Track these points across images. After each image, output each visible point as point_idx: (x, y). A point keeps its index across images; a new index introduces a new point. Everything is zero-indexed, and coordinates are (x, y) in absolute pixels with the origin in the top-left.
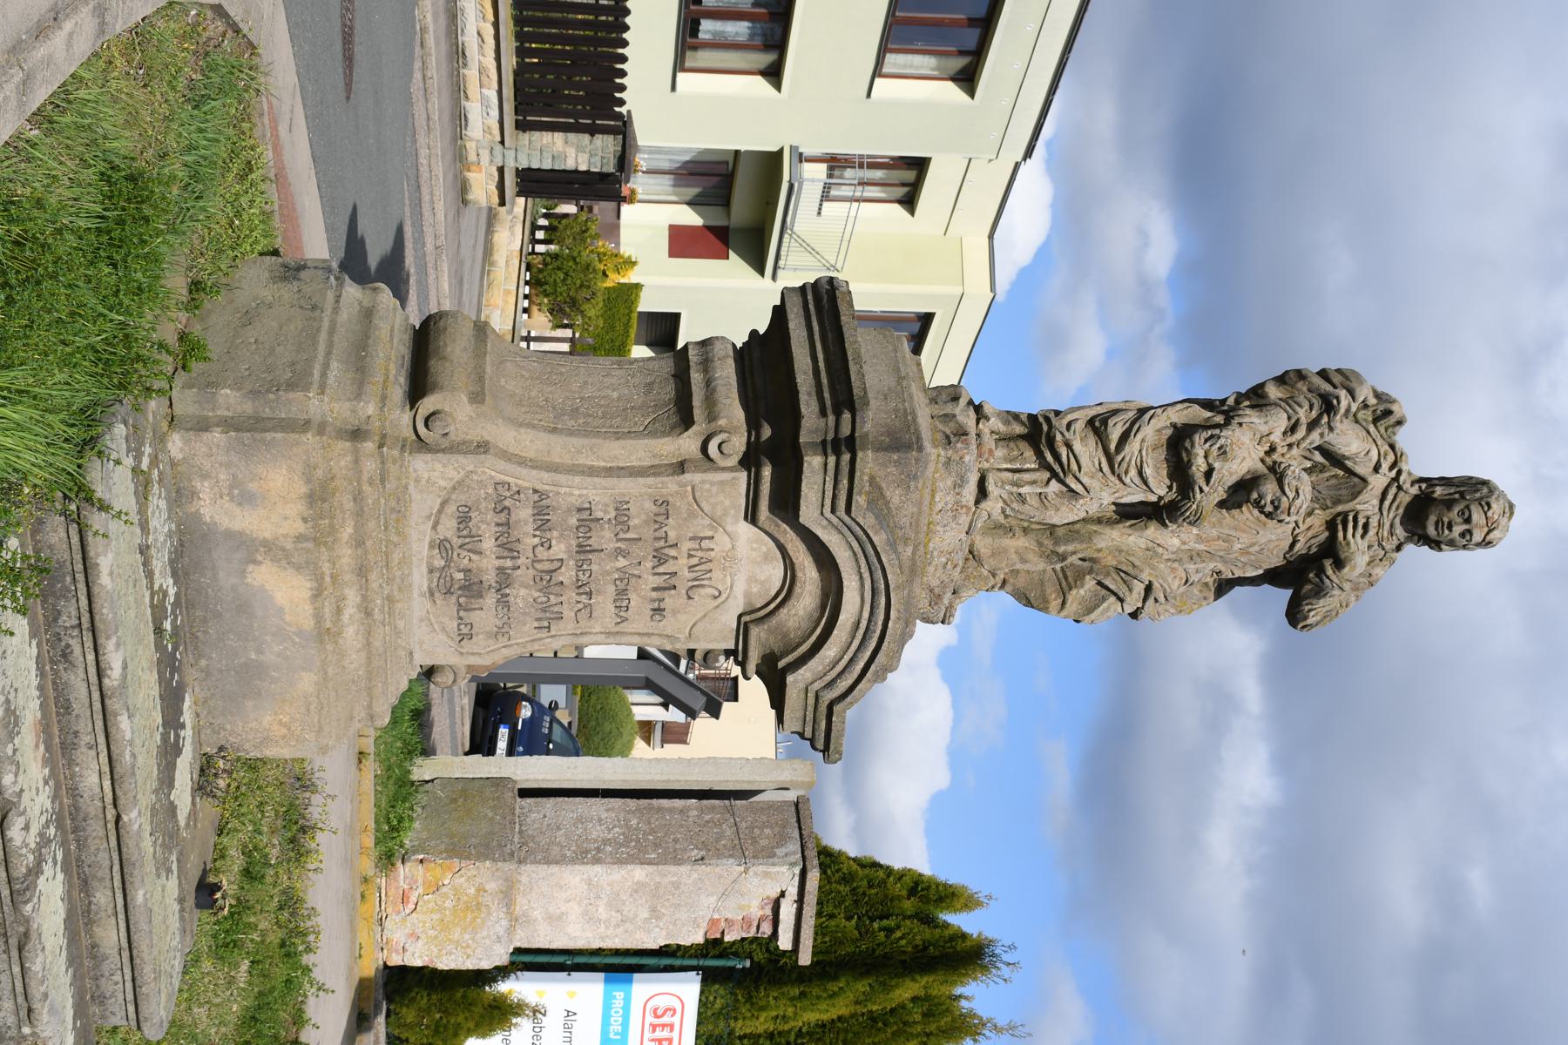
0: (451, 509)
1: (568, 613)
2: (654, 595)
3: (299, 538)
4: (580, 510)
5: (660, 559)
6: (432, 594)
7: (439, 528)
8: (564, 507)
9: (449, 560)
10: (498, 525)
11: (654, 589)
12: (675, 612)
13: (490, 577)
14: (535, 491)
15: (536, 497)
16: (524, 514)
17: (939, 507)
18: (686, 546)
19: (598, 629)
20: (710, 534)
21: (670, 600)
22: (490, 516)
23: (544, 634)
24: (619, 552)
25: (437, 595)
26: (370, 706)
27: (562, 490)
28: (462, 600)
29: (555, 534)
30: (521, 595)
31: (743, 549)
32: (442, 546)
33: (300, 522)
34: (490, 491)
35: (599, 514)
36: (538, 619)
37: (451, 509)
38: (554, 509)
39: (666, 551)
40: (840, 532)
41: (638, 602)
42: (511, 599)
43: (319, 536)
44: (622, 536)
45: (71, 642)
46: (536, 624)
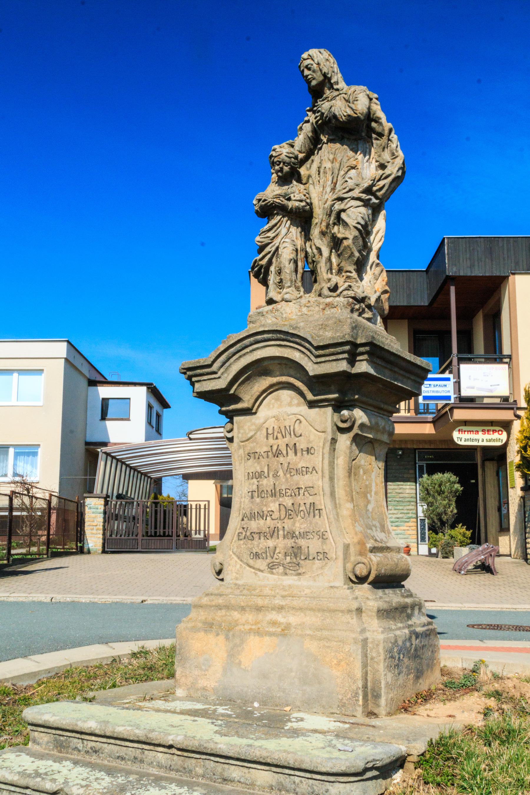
0: (251, 562)
1: (311, 499)
2: (299, 454)
3: (227, 638)
4: (252, 497)
5: (278, 454)
6: (300, 574)
7: (262, 568)
8: (251, 505)
9: (279, 564)
10: (260, 539)
11: (296, 453)
12: (309, 442)
13: (290, 542)
14: (243, 520)
15: (245, 519)
16: (254, 525)
17: (274, 319)
18: (271, 441)
19: (320, 483)
20: (265, 430)
21: (302, 445)
22: (255, 542)
23: (324, 512)
24: (276, 476)
25: (299, 571)
26: (342, 611)
27: (242, 506)
28: (303, 558)
29: (264, 509)
30: (299, 525)
31: (274, 412)
32: (271, 567)
33: (218, 637)
34: (242, 542)
35: (255, 487)
36: (314, 516)
37: (251, 562)
38: (251, 510)
39: (274, 451)
40: (230, 366)
41: (301, 462)
42: (302, 531)
43: (228, 630)
44: (266, 474)
45: (89, 746)
46: (317, 517)
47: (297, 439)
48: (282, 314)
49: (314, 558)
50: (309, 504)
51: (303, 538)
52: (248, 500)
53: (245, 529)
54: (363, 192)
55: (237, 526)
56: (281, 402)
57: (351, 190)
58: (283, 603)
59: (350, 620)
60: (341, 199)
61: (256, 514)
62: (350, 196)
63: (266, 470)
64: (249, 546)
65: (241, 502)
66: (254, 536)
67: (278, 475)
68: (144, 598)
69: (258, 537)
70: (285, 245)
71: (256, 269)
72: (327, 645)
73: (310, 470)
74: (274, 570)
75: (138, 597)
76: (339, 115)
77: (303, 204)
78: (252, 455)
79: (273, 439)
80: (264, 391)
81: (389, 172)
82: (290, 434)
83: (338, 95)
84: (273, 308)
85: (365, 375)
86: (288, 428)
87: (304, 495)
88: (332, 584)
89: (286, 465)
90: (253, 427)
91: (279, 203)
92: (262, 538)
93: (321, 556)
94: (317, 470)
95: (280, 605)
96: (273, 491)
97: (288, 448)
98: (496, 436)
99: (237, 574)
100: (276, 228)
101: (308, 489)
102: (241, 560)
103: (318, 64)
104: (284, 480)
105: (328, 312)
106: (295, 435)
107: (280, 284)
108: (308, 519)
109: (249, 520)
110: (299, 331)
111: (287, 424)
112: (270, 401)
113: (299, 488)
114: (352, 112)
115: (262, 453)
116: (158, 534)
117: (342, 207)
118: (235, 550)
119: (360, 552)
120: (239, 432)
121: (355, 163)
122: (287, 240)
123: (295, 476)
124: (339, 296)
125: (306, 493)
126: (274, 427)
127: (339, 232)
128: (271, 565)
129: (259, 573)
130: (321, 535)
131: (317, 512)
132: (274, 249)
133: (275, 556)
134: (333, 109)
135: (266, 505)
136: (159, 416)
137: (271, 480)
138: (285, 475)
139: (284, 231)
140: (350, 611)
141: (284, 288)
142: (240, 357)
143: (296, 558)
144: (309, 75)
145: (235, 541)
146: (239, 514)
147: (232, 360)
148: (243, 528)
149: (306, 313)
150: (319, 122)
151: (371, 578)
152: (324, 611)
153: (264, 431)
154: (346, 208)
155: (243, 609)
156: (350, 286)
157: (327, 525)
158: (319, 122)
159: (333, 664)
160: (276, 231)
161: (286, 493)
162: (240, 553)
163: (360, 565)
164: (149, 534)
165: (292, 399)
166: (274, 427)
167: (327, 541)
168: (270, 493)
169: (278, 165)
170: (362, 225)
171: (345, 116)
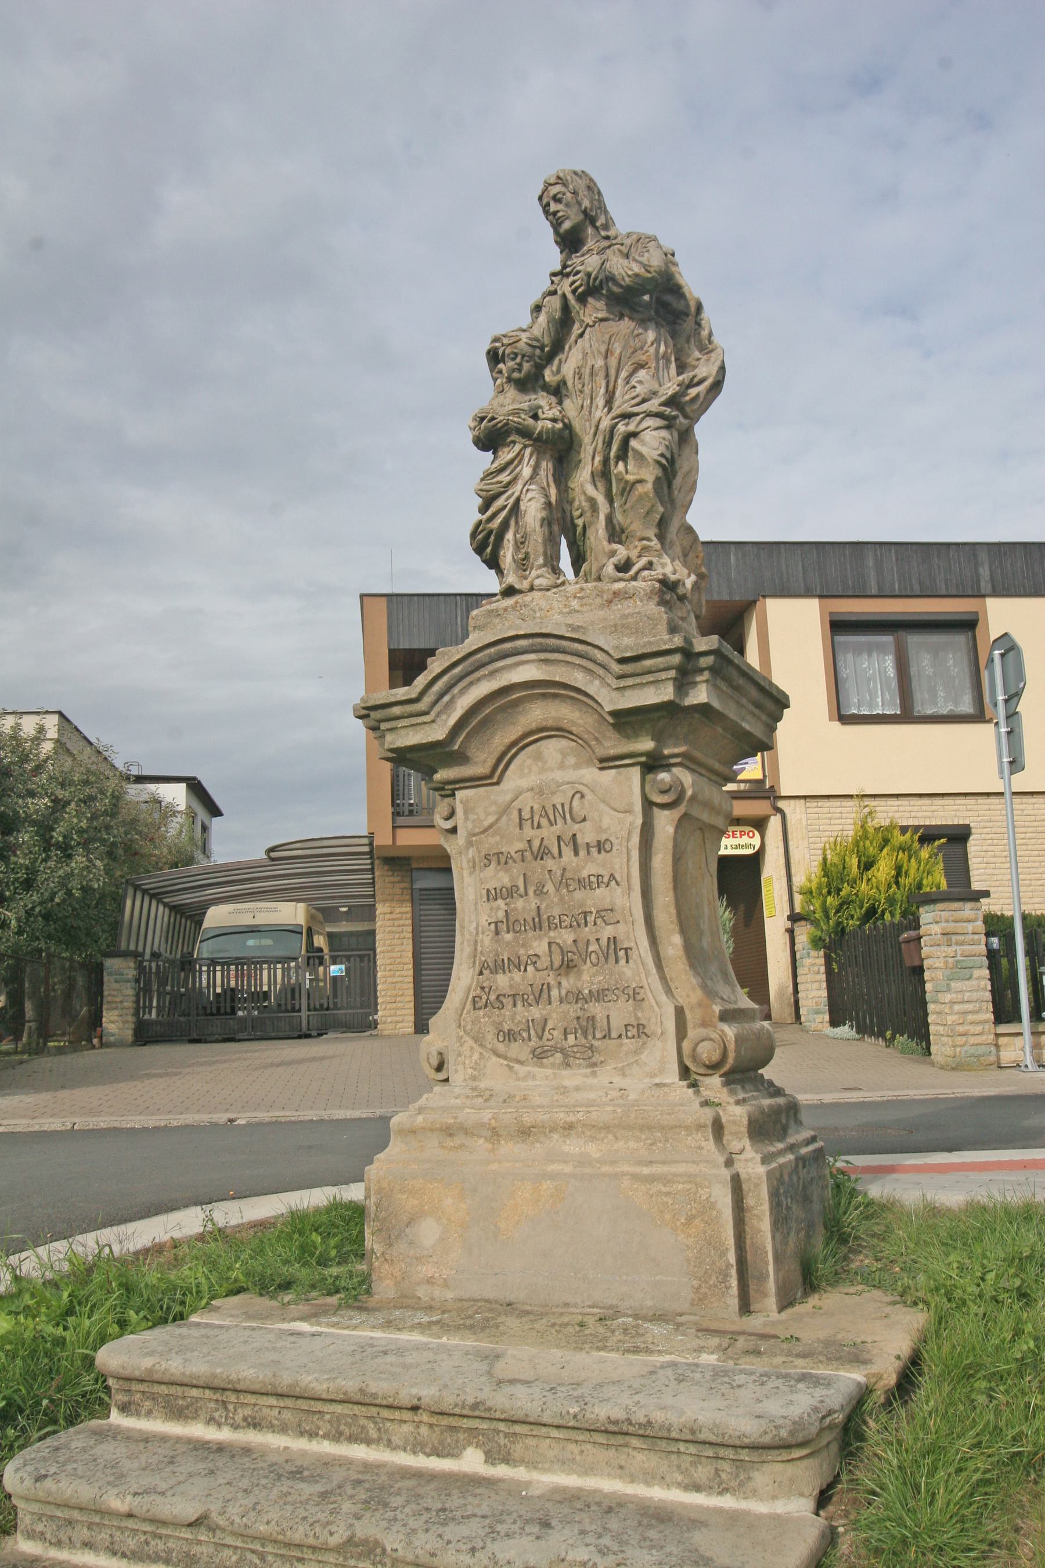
0: (501, 1047)
1: (608, 932)
2: (582, 853)
4: (497, 933)
5: (542, 853)
6: (595, 1065)
9: (555, 1049)
10: (515, 1005)
11: (576, 854)
12: (600, 830)
13: (573, 1010)
14: (481, 973)
15: (485, 972)
18: (529, 832)
21: (587, 835)
22: (507, 1012)
23: (634, 955)
24: (540, 892)
25: (594, 1060)
27: (479, 948)
29: (522, 952)
34: (481, 1013)
35: (501, 915)
36: (617, 961)
37: (501, 1047)
38: (497, 955)
47: (577, 826)
48: (534, 611)
49: (620, 1036)
50: (606, 940)
51: (598, 1000)
52: (489, 938)
53: (487, 990)
54: (662, 404)
55: (471, 985)
56: (545, 763)
57: (644, 401)
58: (571, 1118)
59: (703, 1144)
60: (626, 416)
61: (506, 962)
62: (645, 409)
63: (521, 884)
64: (496, 1018)
65: (476, 941)
66: (505, 1001)
67: (545, 890)
68: (232, 1116)
69: (512, 1003)
70: (530, 495)
71: (480, 536)
72: (664, 1189)
73: (606, 880)
74: (545, 1060)
75: (220, 1115)
76: (620, 274)
77: (559, 425)
78: (498, 858)
79: (533, 828)
80: (513, 744)
81: (704, 374)
82: (564, 818)
83: (609, 247)
84: (516, 603)
85: (704, 709)
86: (559, 807)
87: (595, 924)
88: (657, 1080)
89: (559, 873)
90: (493, 808)
91: (519, 423)
92: (519, 1004)
93: (633, 1032)
94: (618, 879)
95: (566, 1122)
96: (537, 920)
97: (562, 843)
98: (745, 840)
99: (475, 1069)
100: (512, 467)
101: (603, 913)
102: (481, 1045)
103: (575, 193)
104: (556, 900)
105: (617, 607)
106: (572, 819)
107: (523, 564)
108: (606, 966)
109: (492, 973)
110: (584, 633)
111: (558, 800)
112: (524, 761)
113: (585, 913)
114: (643, 270)
115: (513, 854)
116: (222, 1011)
117: (632, 427)
118: (469, 1027)
119: (703, 1021)
120: (467, 819)
121: (644, 358)
122: (533, 487)
123: (577, 891)
124: (634, 578)
125: (599, 921)
126: (532, 808)
127: (627, 472)
128: (539, 1050)
129: (517, 1066)
130: (631, 993)
131: (622, 953)
132: (512, 501)
133: (546, 1034)
134: (608, 265)
135: (523, 946)
136: (205, 828)
137: (533, 902)
138: (558, 890)
139: (527, 471)
140: (700, 1127)
141: (532, 569)
142: (471, 684)
143: (586, 1038)
144: (558, 211)
145: (469, 1012)
146: (474, 963)
147: (456, 690)
148: (483, 988)
149: (577, 608)
150: (580, 290)
151: (726, 1068)
152: (650, 1128)
153: (515, 815)
154: (638, 430)
155: (495, 1134)
156: (651, 563)
157: (643, 976)
158: (580, 290)
159: (678, 1224)
160: (512, 472)
161: (560, 922)
162: (478, 1032)
163: (705, 1043)
164: (208, 1011)
165: (564, 755)
166: (532, 808)
167: (645, 1004)
168: (532, 924)
169: (513, 359)
170: (667, 459)
171: (629, 276)
